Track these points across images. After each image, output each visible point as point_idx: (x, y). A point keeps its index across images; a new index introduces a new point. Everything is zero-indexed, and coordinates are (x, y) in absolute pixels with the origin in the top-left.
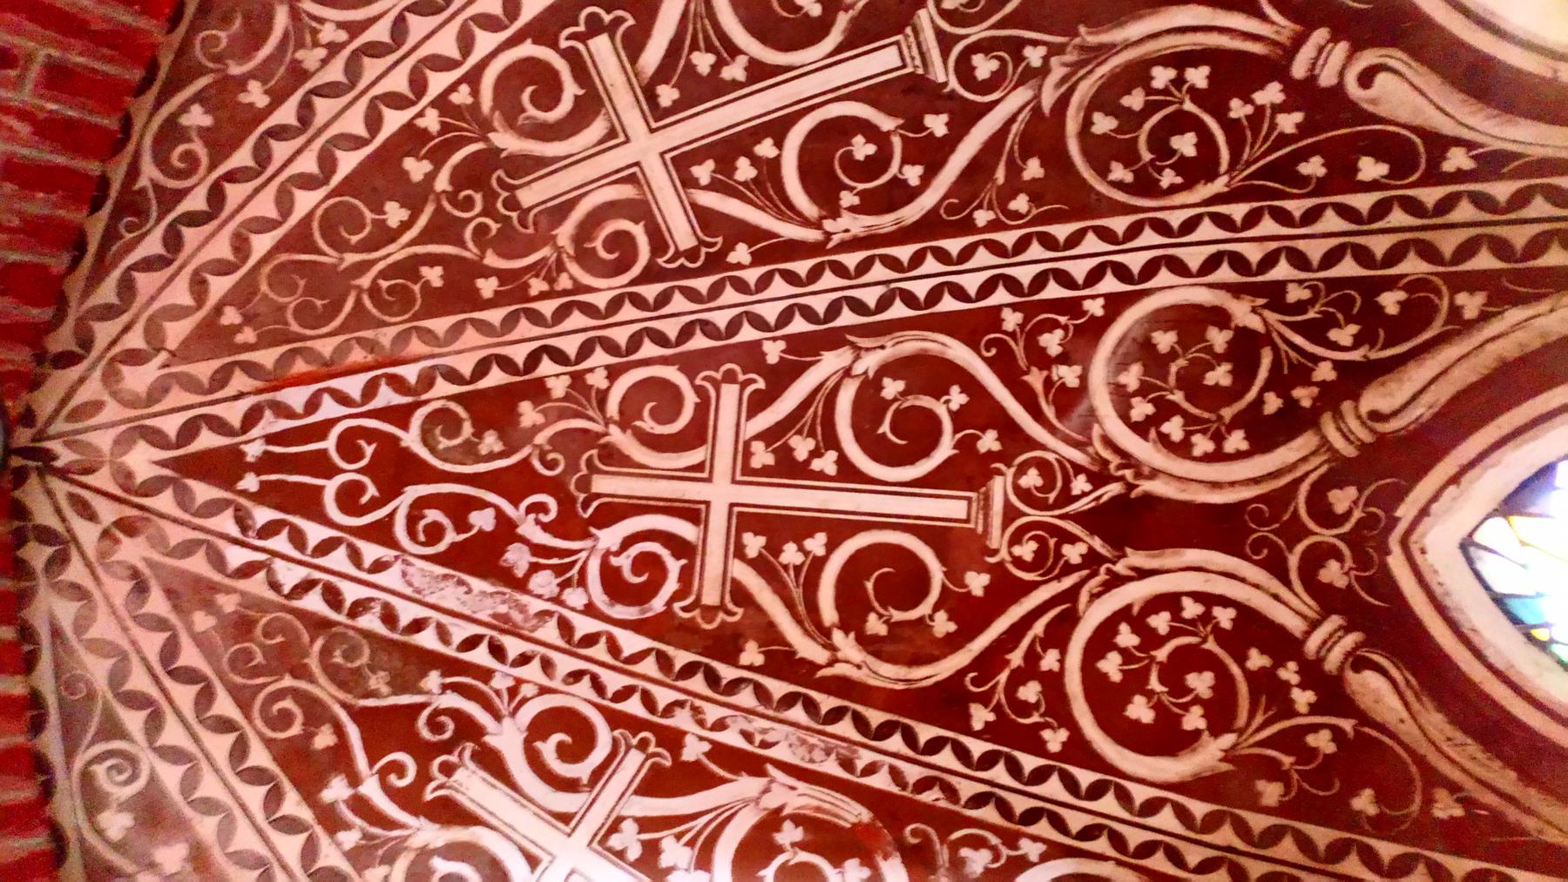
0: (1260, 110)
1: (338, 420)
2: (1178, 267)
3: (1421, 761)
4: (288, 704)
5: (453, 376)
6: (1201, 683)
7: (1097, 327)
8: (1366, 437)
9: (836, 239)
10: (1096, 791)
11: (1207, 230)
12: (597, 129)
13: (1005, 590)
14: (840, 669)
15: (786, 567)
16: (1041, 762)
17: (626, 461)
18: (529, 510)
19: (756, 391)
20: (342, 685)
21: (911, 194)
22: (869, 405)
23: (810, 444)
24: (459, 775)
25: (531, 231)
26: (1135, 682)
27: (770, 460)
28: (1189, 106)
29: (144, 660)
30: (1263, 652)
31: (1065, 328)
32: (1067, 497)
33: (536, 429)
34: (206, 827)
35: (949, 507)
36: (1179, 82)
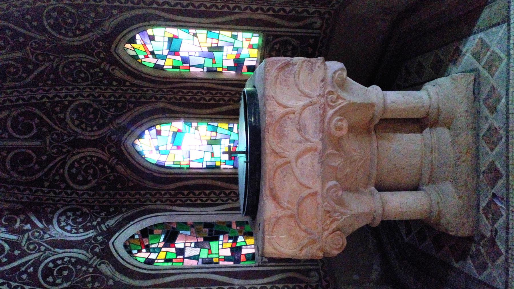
2: (82, 96)
3: (127, 178)
6: (91, 171)
7: (67, 107)
10: (72, 194)
13: (50, 158)
16: (60, 190)
21: (24, 79)
26: (78, 173)
32: (63, 140)
36: (81, 65)
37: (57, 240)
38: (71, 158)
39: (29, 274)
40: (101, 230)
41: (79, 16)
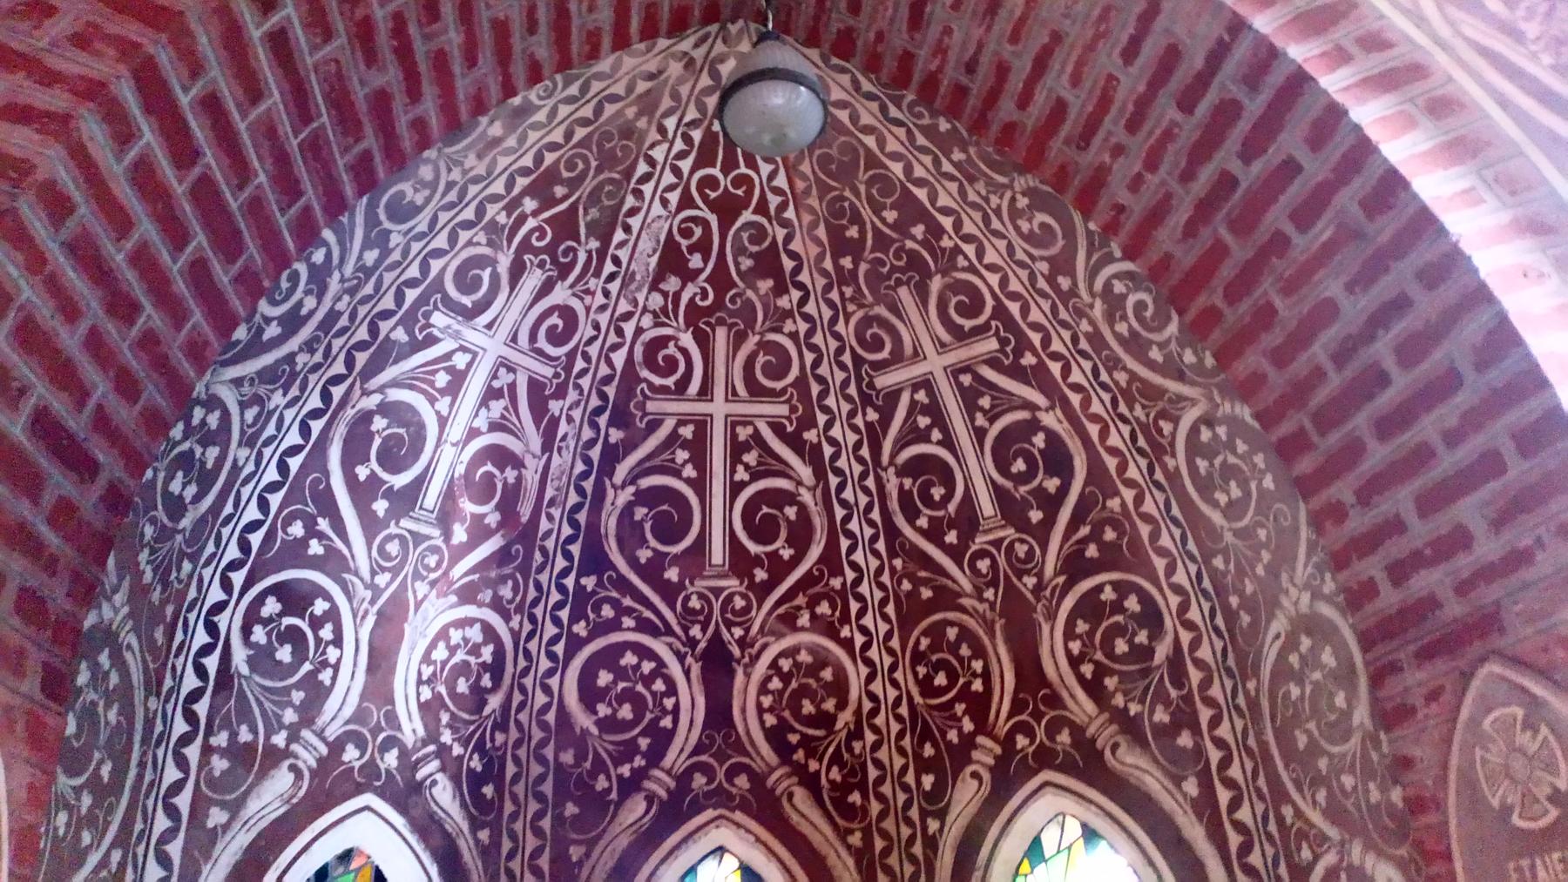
0: (960, 720)
1: (758, 173)
2: (870, 678)
3: (599, 837)
4: (581, 166)
5: (788, 239)
6: (626, 712)
7: (833, 634)
8: (778, 791)
9: (883, 474)
10: (552, 656)
11: (892, 693)
12: (945, 337)
13: (669, 592)
14: (610, 492)
15: (673, 453)
16: (565, 622)
17: (736, 348)
18: (704, 290)
19: (785, 427)
20: (591, 194)
21: (911, 521)
22: (779, 499)
23: (753, 463)
24: (539, 272)
25: (883, 291)
26: (621, 673)
27: (742, 438)
28: (961, 681)
29: (608, 86)
30: (649, 745)
31: (833, 615)
32: (729, 625)
33: (756, 290)
34: (511, 142)
35: (718, 553)
36: (975, 675)
37: (405, 619)
38: (672, 649)
39: (303, 543)
40: (418, 761)
41: (1146, 673)
